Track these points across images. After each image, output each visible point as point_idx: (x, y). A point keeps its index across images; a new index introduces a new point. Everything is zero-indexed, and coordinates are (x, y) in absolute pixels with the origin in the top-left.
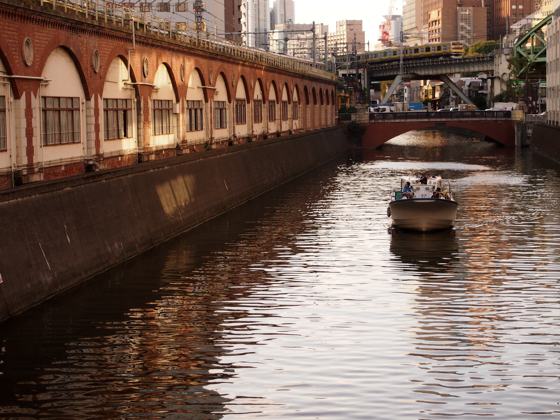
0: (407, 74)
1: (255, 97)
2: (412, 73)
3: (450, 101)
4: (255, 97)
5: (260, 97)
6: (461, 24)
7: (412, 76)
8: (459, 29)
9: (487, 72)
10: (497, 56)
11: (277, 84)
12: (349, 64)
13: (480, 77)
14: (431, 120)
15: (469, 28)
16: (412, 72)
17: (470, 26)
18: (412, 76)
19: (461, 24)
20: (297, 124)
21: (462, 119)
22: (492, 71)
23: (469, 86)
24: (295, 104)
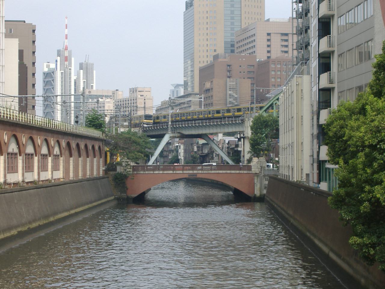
0: (174, 133)
1: (55, 153)
2: (179, 133)
3: (214, 156)
4: (55, 153)
5: (58, 153)
6: (230, 92)
7: (179, 135)
8: (228, 97)
9: (240, 133)
10: (247, 119)
11: (49, 142)
12: (230, 123)
13: (236, 136)
14: (185, 172)
15: (236, 96)
16: (178, 131)
17: (237, 94)
18: (179, 135)
19: (230, 92)
20: (59, 175)
21: (210, 172)
22: (243, 132)
23: (228, 144)
24: (56, 157)
